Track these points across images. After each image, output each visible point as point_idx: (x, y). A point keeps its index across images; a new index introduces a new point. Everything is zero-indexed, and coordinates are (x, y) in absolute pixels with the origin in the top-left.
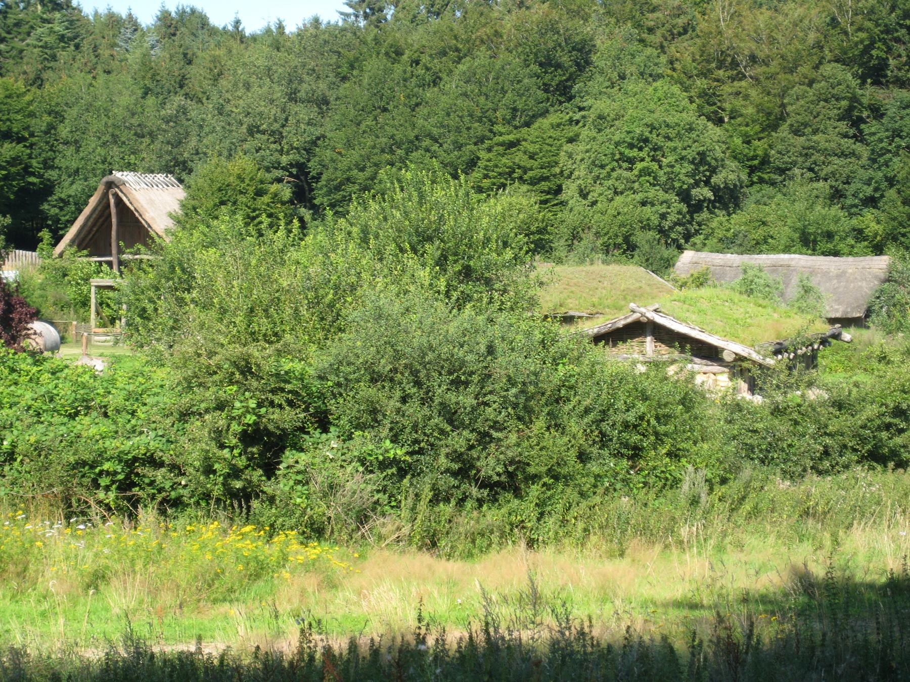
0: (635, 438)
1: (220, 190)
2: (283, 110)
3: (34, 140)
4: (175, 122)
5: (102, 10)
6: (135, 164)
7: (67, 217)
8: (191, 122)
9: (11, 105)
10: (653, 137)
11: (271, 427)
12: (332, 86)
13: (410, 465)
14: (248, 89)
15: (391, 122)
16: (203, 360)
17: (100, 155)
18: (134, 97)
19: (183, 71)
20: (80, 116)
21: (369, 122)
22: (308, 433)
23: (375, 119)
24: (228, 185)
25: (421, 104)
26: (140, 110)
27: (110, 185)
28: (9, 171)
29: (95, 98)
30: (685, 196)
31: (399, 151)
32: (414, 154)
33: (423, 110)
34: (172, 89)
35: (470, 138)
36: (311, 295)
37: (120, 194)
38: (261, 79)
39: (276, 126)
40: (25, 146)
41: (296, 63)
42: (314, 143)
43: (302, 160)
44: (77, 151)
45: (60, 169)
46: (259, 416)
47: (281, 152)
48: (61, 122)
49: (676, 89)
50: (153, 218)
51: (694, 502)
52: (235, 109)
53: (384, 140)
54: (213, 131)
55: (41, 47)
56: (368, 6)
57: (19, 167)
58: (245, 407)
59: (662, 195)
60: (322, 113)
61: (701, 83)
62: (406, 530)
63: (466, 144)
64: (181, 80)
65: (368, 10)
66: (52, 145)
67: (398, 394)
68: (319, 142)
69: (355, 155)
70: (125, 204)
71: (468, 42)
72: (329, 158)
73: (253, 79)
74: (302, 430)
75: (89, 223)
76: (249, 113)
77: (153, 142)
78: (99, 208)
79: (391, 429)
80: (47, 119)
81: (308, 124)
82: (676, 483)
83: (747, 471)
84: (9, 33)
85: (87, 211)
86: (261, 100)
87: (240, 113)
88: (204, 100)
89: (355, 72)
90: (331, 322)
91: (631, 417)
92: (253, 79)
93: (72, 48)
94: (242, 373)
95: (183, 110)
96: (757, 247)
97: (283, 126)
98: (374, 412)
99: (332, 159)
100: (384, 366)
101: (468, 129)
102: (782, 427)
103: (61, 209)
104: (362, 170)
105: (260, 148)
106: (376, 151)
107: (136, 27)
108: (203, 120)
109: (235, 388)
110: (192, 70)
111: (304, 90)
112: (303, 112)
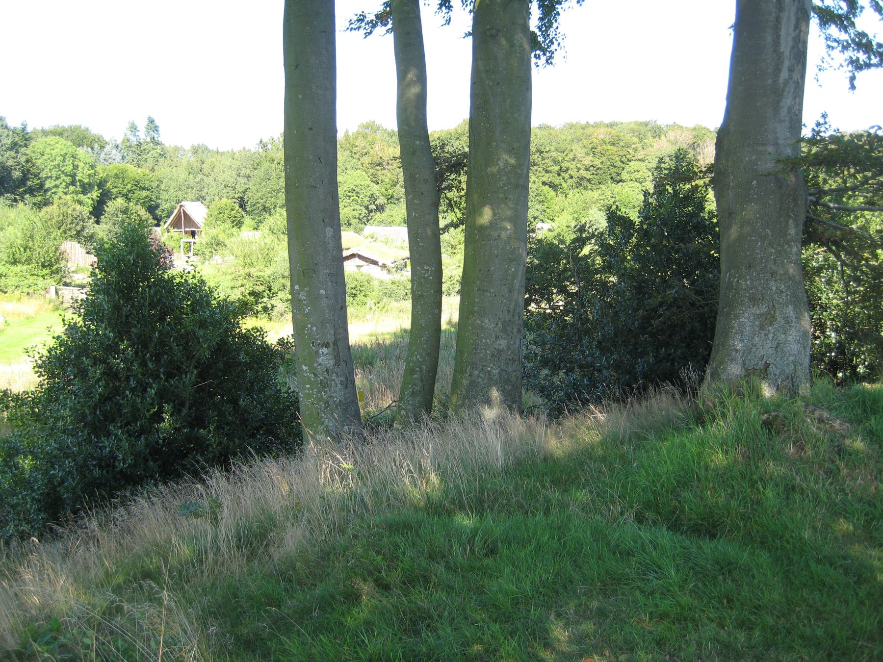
0: (354, 292)
10: (356, 189)
27: (181, 206)
30: (367, 208)
42: (246, 190)
49: (364, 173)
51: (371, 309)
52: (220, 179)
58: (249, 286)
59: (360, 208)
61: (372, 171)
69: (260, 194)
82: (366, 303)
83: (385, 299)
86: (229, 176)
91: (353, 286)
102: (394, 287)
110: (204, 166)
112: (242, 180)
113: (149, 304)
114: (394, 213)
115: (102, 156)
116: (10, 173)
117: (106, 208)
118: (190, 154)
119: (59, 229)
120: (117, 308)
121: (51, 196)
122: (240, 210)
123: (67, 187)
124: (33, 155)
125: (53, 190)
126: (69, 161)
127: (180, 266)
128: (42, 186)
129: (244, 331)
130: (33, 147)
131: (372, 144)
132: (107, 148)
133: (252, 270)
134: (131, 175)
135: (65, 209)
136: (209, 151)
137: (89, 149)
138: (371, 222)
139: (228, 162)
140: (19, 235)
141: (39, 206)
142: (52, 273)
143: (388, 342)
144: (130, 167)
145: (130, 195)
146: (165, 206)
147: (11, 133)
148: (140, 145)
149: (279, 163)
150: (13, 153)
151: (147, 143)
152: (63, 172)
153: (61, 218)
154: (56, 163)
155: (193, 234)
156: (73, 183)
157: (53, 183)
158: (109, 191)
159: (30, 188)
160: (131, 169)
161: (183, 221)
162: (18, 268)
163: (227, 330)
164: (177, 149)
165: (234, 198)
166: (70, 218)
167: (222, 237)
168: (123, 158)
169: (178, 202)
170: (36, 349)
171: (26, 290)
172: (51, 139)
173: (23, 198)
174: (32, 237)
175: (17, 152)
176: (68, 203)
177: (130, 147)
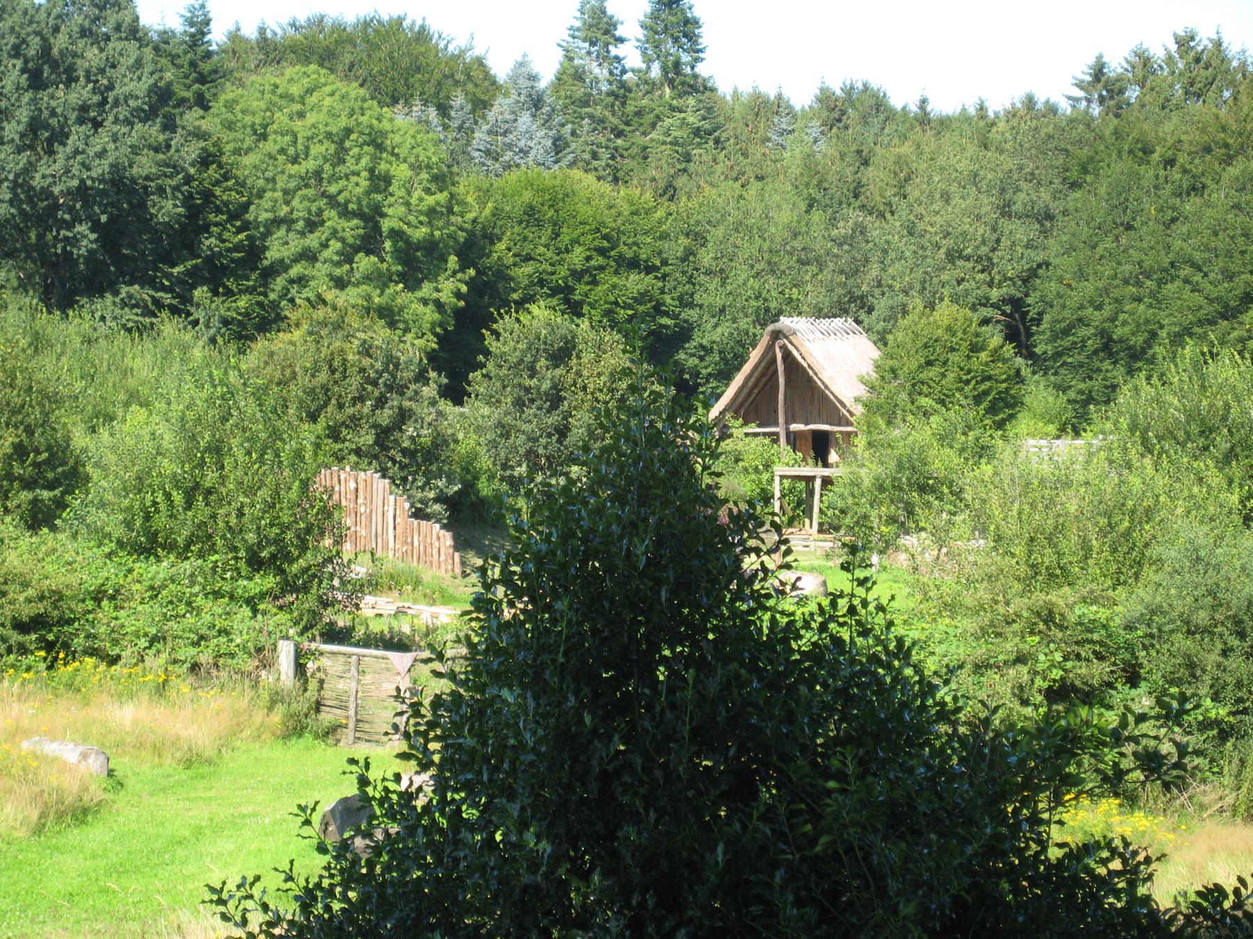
1: (926, 346)
2: (994, 230)
3: (667, 269)
4: (851, 245)
5: (746, 88)
6: (798, 300)
7: (709, 370)
8: (870, 245)
9: (638, 224)
11: (1078, 683)
13: (1232, 727)
14: (947, 202)
15: (1138, 244)
16: (1001, 609)
17: (752, 288)
18: (796, 213)
19: (859, 175)
20: (727, 237)
21: (1108, 243)
22: (1116, 689)
23: (1117, 239)
24: (936, 341)
25: (1177, 219)
26: (804, 229)
27: (776, 335)
28: (636, 310)
29: (747, 213)
31: (1149, 283)
32: (1169, 286)
34: (844, 199)
35: (1244, 265)
36: (1103, 521)
37: (790, 346)
38: (964, 188)
39: (984, 250)
40: (656, 277)
41: (1010, 166)
42: (1033, 273)
43: (1019, 295)
44: (724, 284)
45: (701, 307)
46: (1065, 671)
47: (990, 284)
48: (703, 245)
50: (831, 378)
52: (933, 224)
53: (1128, 267)
54: (902, 257)
55: (671, 143)
56: (1105, 87)
57: (649, 306)
58: (1050, 661)
60: (1045, 232)
62: (1230, 800)
63: (1240, 273)
64: (856, 188)
65: (1104, 93)
66: (691, 276)
67: (1219, 646)
68: (1041, 272)
69: (1089, 288)
70: (794, 359)
71: (1240, 134)
72: (1055, 293)
73: (954, 188)
74: (1110, 685)
75: (750, 384)
76: (948, 234)
77: (821, 270)
78: (763, 364)
79: (1212, 686)
80: (684, 241)
81: (1027, 246)
84: (627, 124)
85: (747, 368)
86: (965, 214)
87: (936, 233)
88: (888, 215)
89: (1089, 178)
90: (1130, 561)
92: (954, 188)
93: (711, 143)
94: (1046, 622)
95: (861, 229)
97: (994, 250)
98: (1191, 666)
99: (1058, 294)
100: (1202, 617)
101: (1243, 253)
103: (702, 358)
104: (1099, 308)
105: (963, 280)
106: (1115, 282)
107: (790, 111)
108: (888, 242)
109: (1037, 639)
110: (870, 172)
111: (1020, 202)
112: (1020, 231)
113: (695, 732)
115: (480, 136)
116: (142, 205)
117: (489, 340)
118: (815, 128)
119: (313, 418)
120: (568, 741)
121: (285, 294)
122: (1009, 350)
123: (347, 257)
124: (226, 136)
125: (295, 271)
126: (359, 160)
127: (803, 573)
128: (254, 252)
129: (1054, 853)
130: (229, 106)
132: (500, 108)
133: (1060, 597)
134: (585, 211)
137: (432, 112)
140: (168, 439)
141: (241, 332)
142: (289, 586)
144: (585, 182)
145: (581, 288)
146: (714, 333)
147: (148, 52)
148: (621, 92)
149: (1170, 162)
150: (154, 131)
151: (652, 86)
152: (332, 200)
153: (323, 377)
154: (311, 165)
155: (819, 446)
156: (369, 243)
157: (296, 244)
158: (501, 274)
159: (209, 260)
161: (787, 392)
162: (160, 569)
163: (995, 848)
164: (765, 109)
165: (985, 302)
166: (355, 382)
167: (942, 461)
168: (559, 146)
169: (767, 316)
170: (256, 891)
171: (187, 653)
172: (293, 78)
173: (187, 299)
174: (217, 450)
175: (169, 126)
176: (341, 319)
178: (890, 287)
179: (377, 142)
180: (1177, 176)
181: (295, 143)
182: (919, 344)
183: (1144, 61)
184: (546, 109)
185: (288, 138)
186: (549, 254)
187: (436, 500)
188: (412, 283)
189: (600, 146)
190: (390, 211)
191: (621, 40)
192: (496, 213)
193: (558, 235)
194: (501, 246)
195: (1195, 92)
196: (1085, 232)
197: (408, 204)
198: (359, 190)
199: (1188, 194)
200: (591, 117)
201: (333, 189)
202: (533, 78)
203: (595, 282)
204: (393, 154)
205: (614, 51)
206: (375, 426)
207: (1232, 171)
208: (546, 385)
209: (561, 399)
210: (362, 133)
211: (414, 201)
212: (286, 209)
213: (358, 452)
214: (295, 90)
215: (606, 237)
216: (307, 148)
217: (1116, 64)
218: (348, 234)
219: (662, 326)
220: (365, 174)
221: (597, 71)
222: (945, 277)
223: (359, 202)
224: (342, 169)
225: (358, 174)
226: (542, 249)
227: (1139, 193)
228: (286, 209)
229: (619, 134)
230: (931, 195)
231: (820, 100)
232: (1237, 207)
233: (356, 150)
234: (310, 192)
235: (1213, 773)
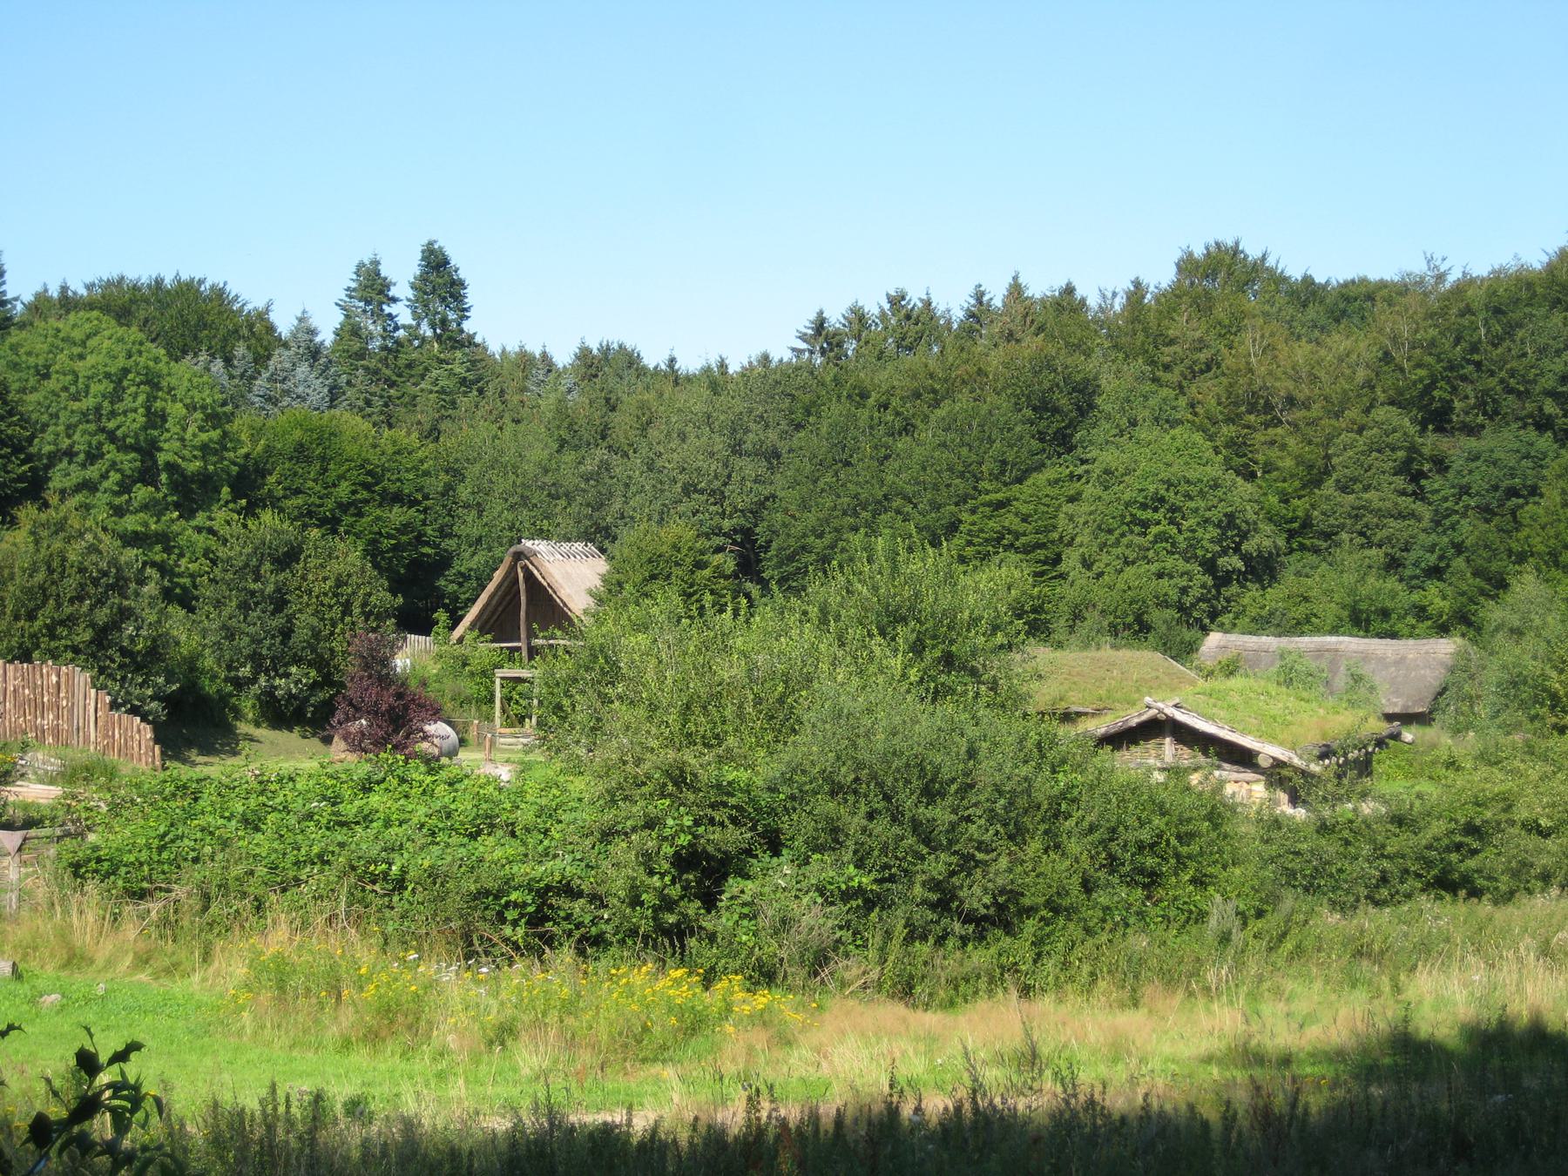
0: (1150, 862)
1: (650, 561)
2: (726, 465)
5: (513, 347)
11: (710, 849)
12: (783, 435)
13: (878, 896)
14: (683, 441)
23: (836, 474)
27: (518, 556)
30: (1209, 566)
33: (894, 464)
39: (717, 484)
42: (762, 504)
44: (480, 516)
47: (723, 515)
49: (1198, 437)
51: (1225, 939)
53: (846, 500)
54: (642, 490)
59: (1182, 565)
61: (1228, 431)
62: (874, 975)
67: (863, 809)
69: (811, 519)
71: (946, 380)
74: (749, 852)
79: (855, 852)
81: (755, 481)
82: (1202, 916)
83: (1289, 900)
84: (400, 376)
85: (491, 587)
86: (697, 453)
90: (781, 720)
91: (1145, 835)
94: (676, 784)
95: (605, 466)
96: (1298, 627)
97: (725, 484)
98: (835, 830)
101: (948, 486)
102: (1330, 847)
103: (461, 585)
104: (820, 536)
108: (630, 477)
109: (668, 802)
110: (616, 418)
112: (749, 468)
114: (1313, 586)
115: (261, 383)
126: (134, 398)
131: (1231, 330)
134: (351, 450)
135: (57, 545)
136: (642, 371)
138: (1226, 619)
139: (697, 401)
143: (1315, 1102)
148: (394, 349)
152: (112, 437)
154: (89, 402)
157: (77, 475)
160: (351, 423)
164: (527, 364)
168: (334, 394)
177: (361, 355)
178: (632, 518)
179: (152, 381)
180: (890, 418)
181: (76, 382)
182: (644, 559)
183: (858, 318)
184: (323, 360)
185: (69, 378)
186: (318, 488)
187: (153, 698)
188: (188, 513)
189: (373, 394)
190: (166, 446)
191: (394, 300)
192: (268, 449)
193: (326, 470)
194: (271, 479)
195: (907, 345)
196: (809, 468)
197: (182, 440)
198: (136, 426)
199: (900, 434)
200: (366, 369)
201: (111, 425)
202: (312, 332)
203: (360, 514)
204: (169, 393)
205: (387, 309)
206: (92, 625)
207: (940, 413)
208: (270, 589)
209: (286, 602)
210: (139, 374)
211: (188, 436)
212: (68, 442)
213: (76, 650)
214: (77, 335)
215: (369, 473)
216: (87, 387)
217: (836, 317)
218: (126, 466)
219: (424, 555)
220: (141, 410)
221: (371, 327)
222: (681, 508)
223: (136, 436)
224: (120, 407)
225: (135, 411)
226: (310, 484)
227: (856, 433)
228: (68, 442)
229: (392, 384)
230: (668, 434)
231: (577, 357)
232: (944, 445)
233: (133, 389)
234: (92, 427)
235: (857, 947)
